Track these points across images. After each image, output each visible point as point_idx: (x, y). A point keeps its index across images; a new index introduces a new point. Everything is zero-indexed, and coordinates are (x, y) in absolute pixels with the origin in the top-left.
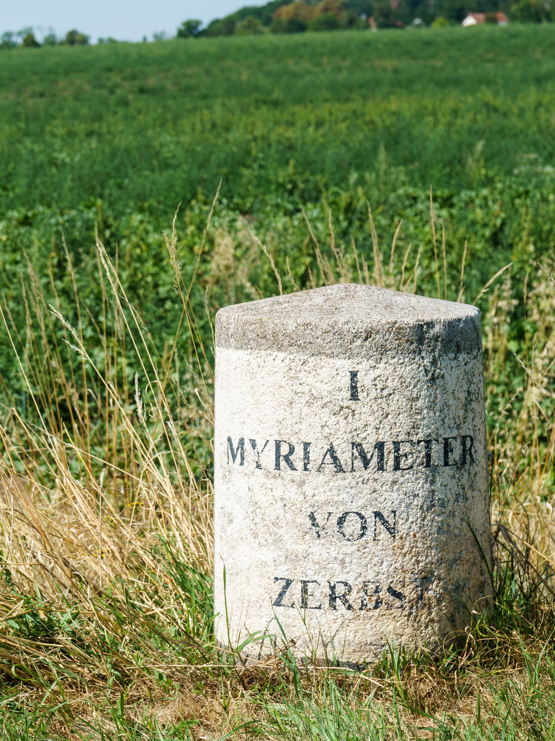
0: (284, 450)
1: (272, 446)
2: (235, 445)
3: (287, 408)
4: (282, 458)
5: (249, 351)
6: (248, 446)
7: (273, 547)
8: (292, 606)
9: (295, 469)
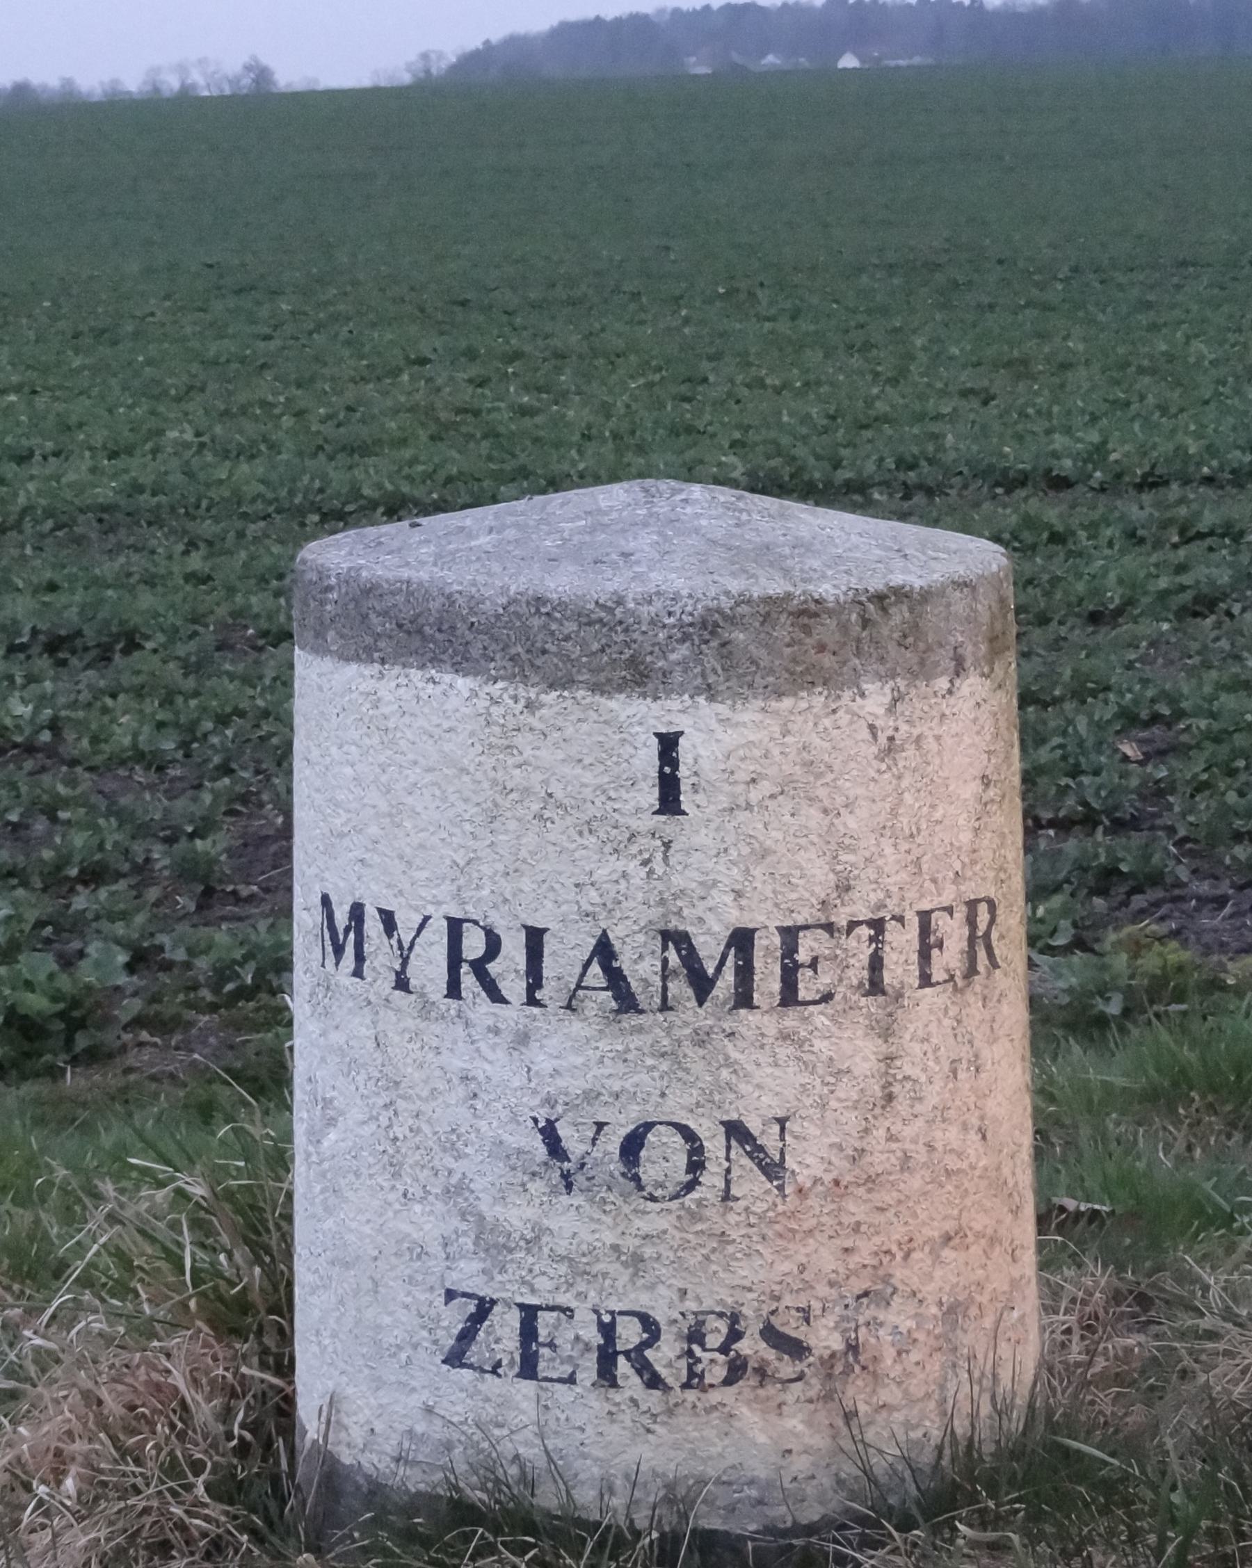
0: (474, 945)
1: (437, 935)
2: (341, 918)
3: (479, 832)
4: (465, 968)
5: (377, 666)
6: (373, 926)
7: (439, 1207)
8: (494, 1371)
9: (503, 1000)
